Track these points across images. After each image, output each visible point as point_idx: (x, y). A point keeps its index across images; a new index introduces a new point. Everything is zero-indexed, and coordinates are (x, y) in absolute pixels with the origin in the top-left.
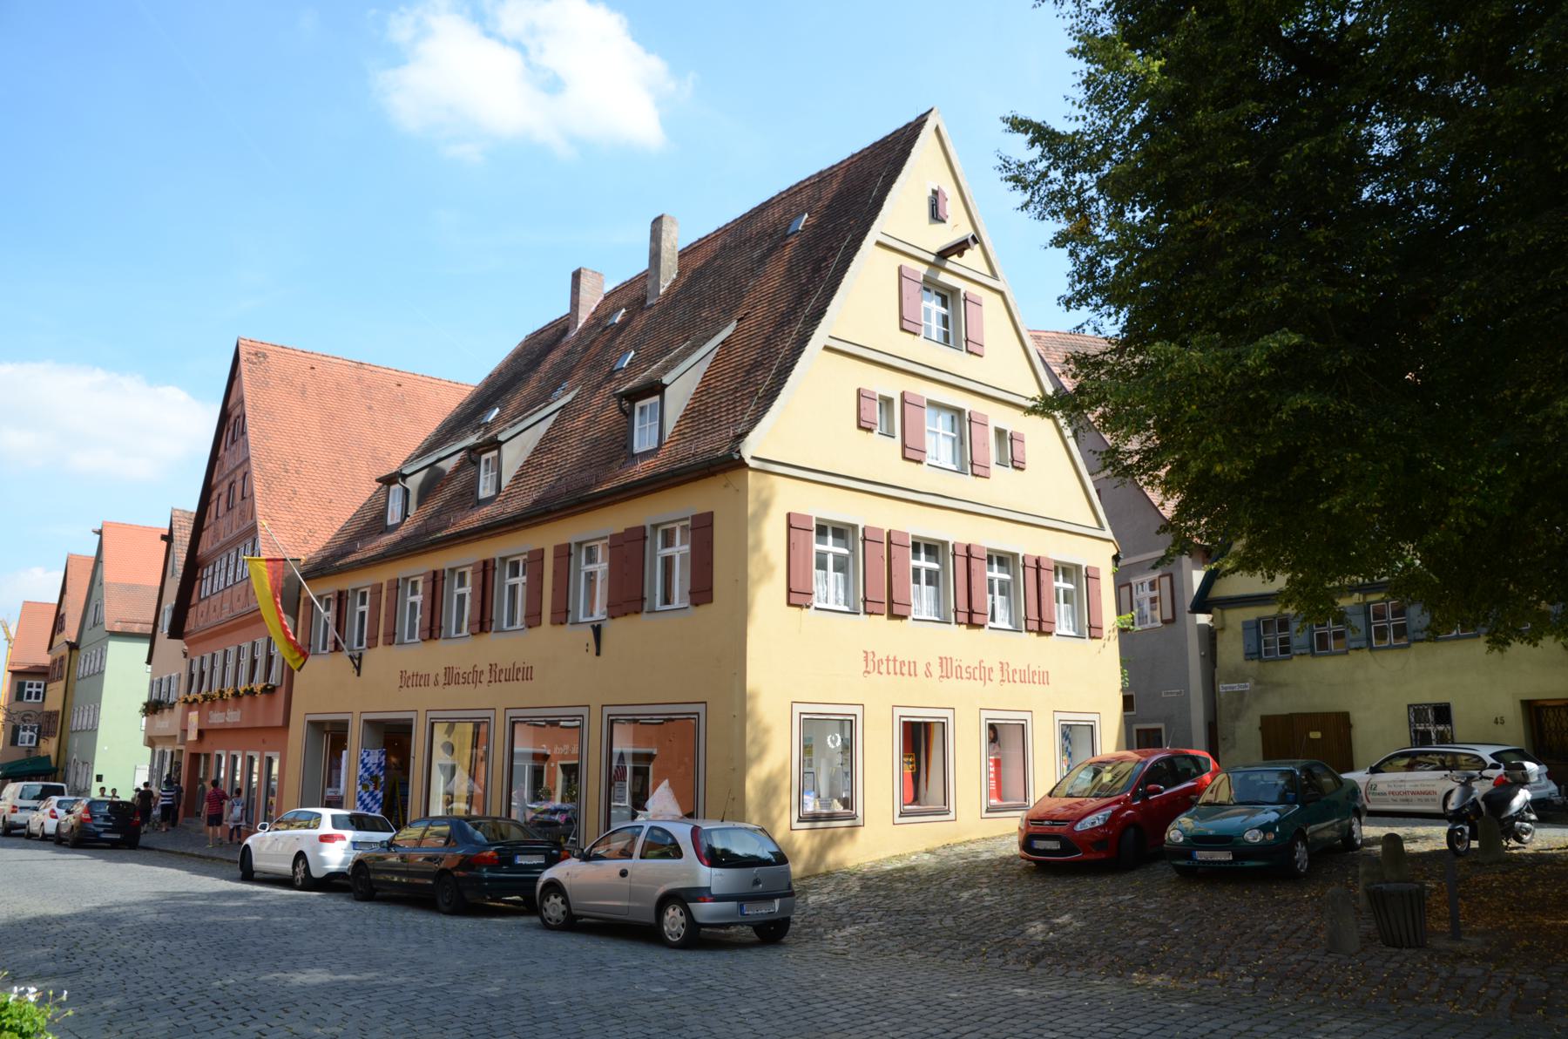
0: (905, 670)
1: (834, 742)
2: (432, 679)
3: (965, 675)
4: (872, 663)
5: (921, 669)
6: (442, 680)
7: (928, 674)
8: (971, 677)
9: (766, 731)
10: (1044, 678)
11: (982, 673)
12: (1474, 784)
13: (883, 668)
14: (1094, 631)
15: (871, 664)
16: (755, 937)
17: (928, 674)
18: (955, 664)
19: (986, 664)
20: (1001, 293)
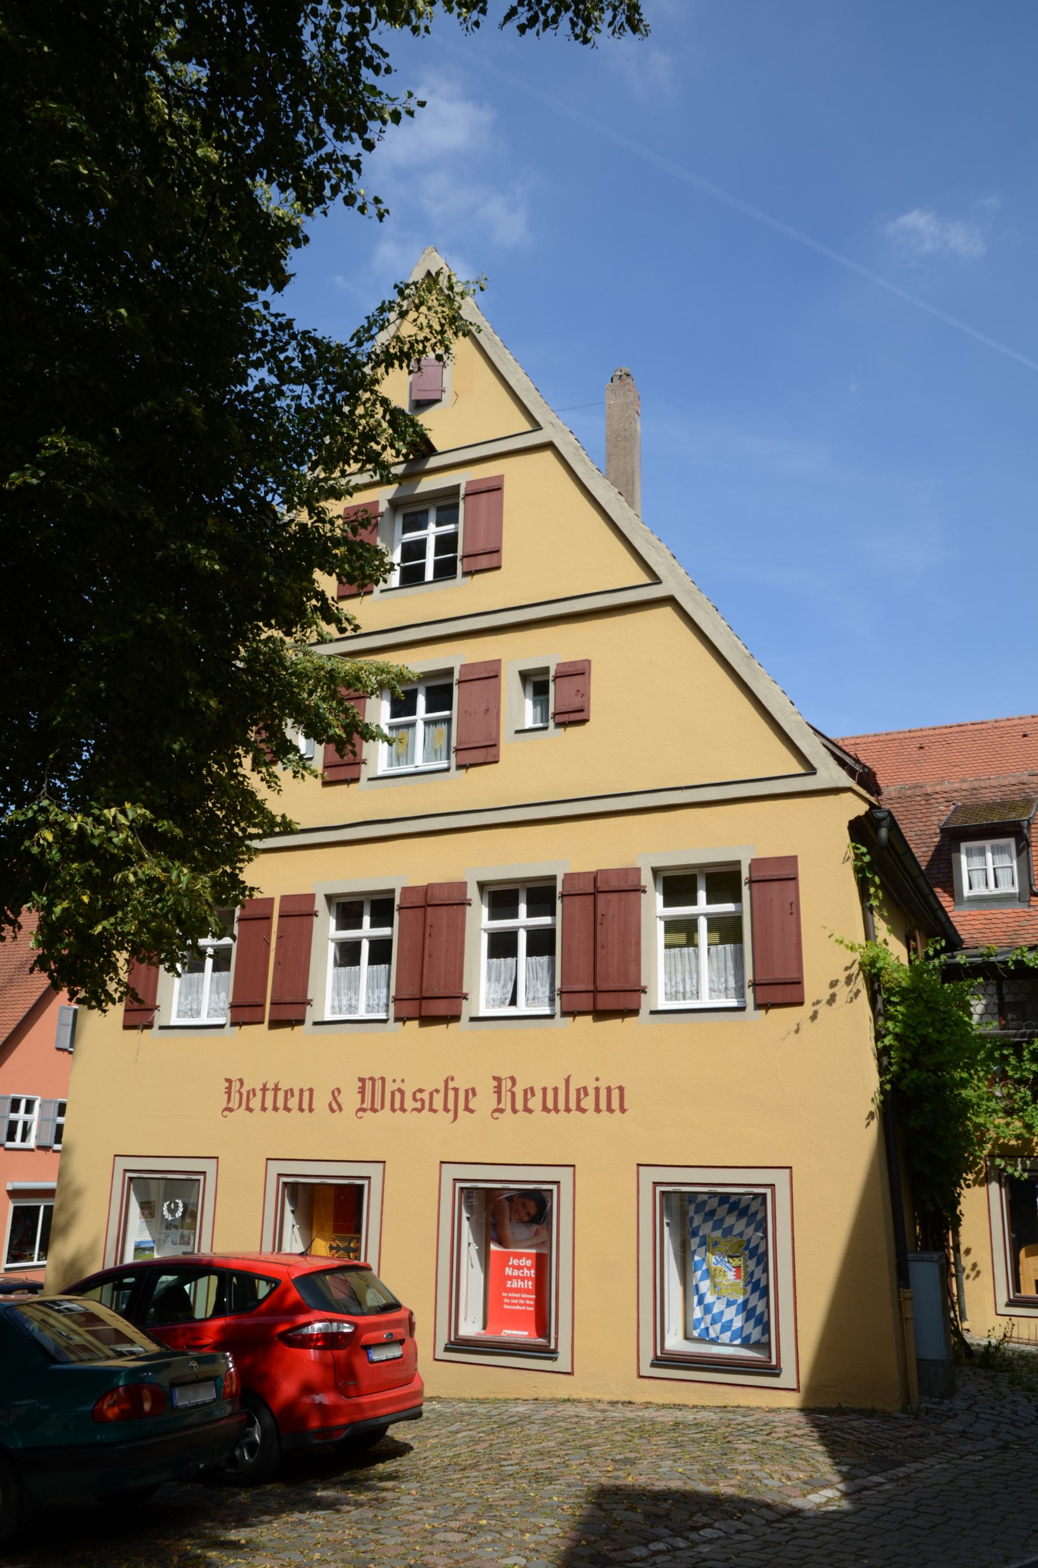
0: (293, 1103)
1: (172, 1212)
2: (322, 1100)
3: (409, 1104)
4: (237, 1095)
5: (322, 1100)
6: (350, 1099)
7: (335, 1106)
8: (425, 1106)
9: (78, 1194)
10: (613, 1100)
11: (456, 1100)
12: (368, 749)
13: (256, 1103)
14: (776, 988)
15: (235, 1097)
16: (765, 1299)
17: (335, 1106)
18: (390, 1087)
19: (462, 1083)
20: (670, 601)
